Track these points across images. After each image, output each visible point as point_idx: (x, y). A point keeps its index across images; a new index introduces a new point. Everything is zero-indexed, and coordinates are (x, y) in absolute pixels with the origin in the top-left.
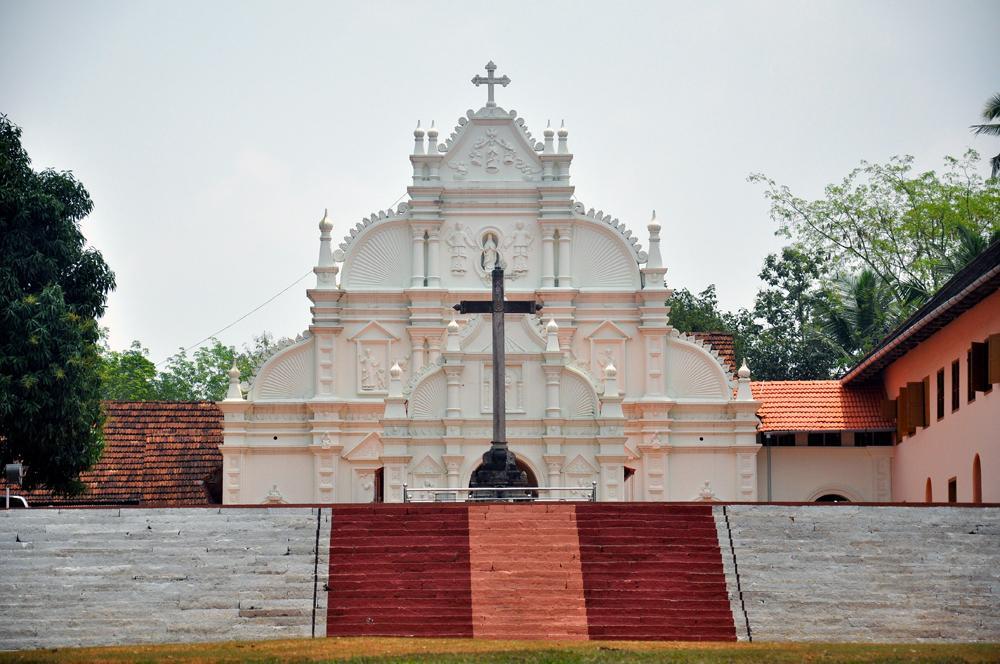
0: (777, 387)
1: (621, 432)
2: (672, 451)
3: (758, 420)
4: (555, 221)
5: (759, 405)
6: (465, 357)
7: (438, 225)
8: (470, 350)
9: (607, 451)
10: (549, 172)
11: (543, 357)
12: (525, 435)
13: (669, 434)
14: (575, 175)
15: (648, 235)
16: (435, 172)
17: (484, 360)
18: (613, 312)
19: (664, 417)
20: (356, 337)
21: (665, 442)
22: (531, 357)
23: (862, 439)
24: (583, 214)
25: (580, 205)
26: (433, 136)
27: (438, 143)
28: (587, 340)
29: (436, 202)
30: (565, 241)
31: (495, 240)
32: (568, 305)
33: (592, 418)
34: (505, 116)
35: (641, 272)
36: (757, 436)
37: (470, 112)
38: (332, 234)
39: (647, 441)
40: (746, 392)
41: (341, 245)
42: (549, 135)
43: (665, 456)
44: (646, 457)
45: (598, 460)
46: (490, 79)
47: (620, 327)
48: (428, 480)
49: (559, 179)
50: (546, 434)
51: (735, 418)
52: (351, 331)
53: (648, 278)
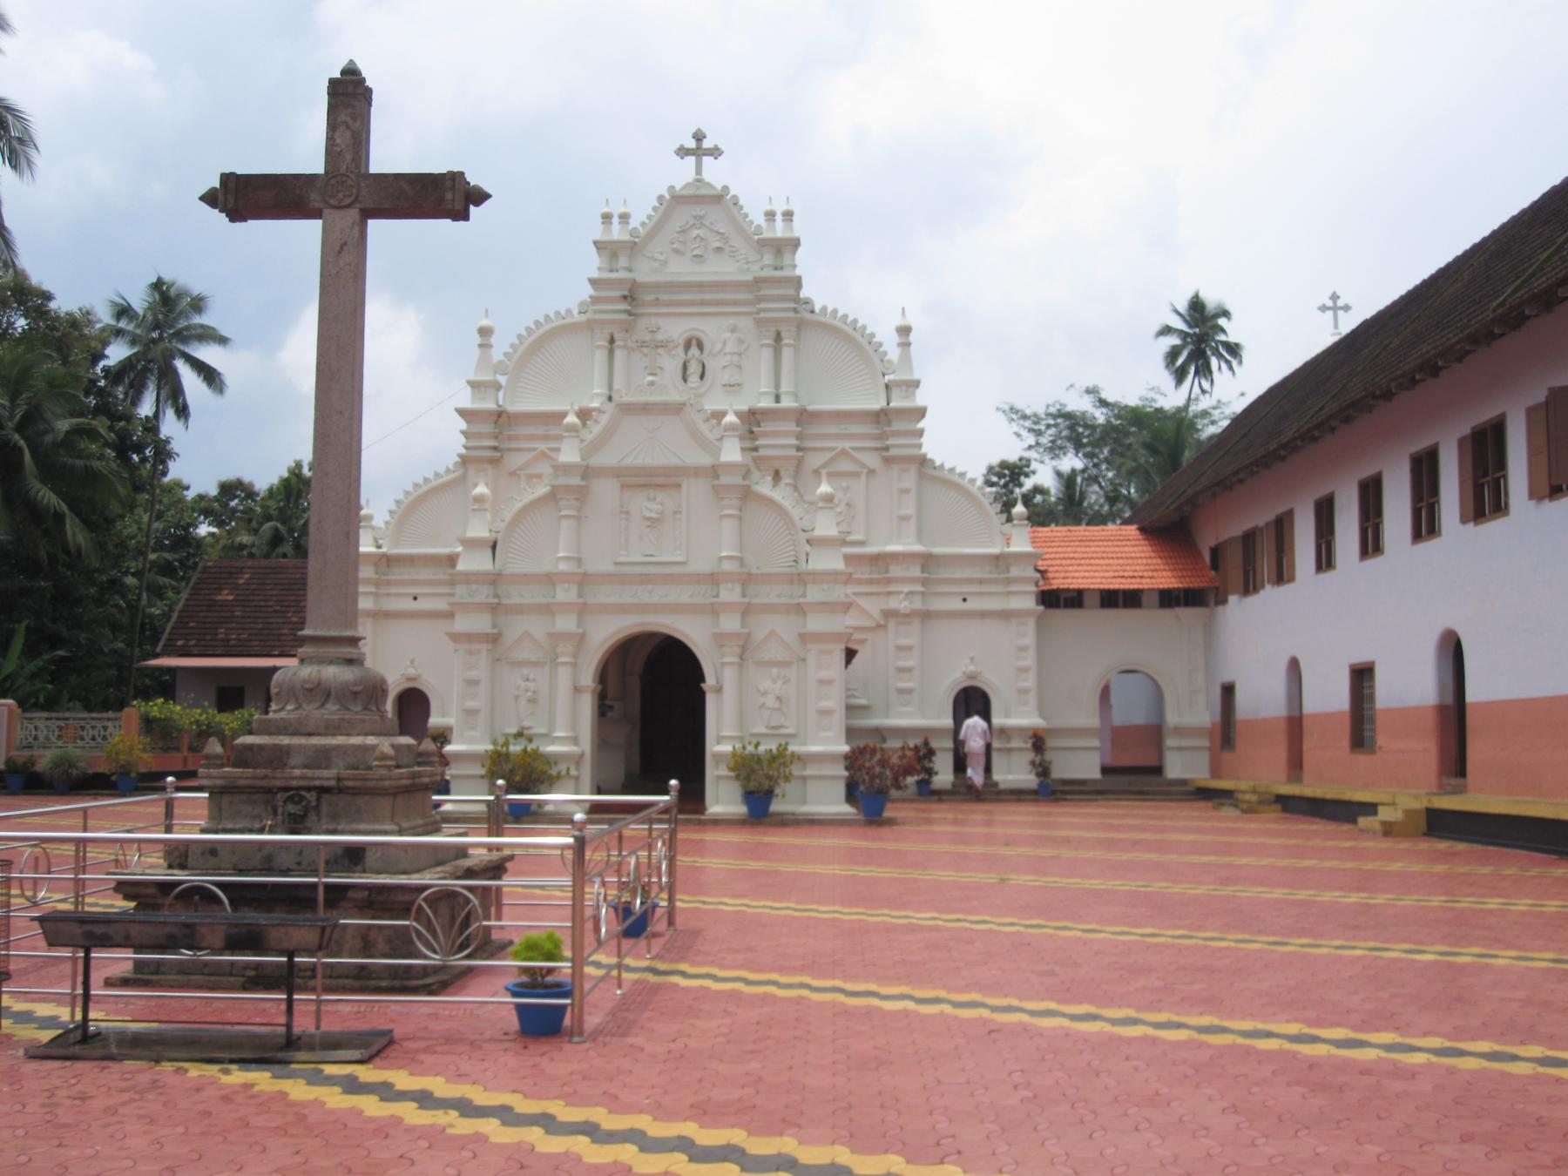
0: (1059, 534)
1: (839, 593)
2: (926, 616)
3: (1038, 575)
4: (775, 320)
5: (1037, 556)
6: (587, 472)
7: (628, 328)
8: (597, 461)
9: (816, 623)
10: (768, 259)
11: (714, 471)
12: (685, 598)
13: (923, 594)
14: (804, 263)
15: (896, 338)
16: (623, 261)
17: (618, 476)
18: (851, 437)
19: (916, 571)
20: (521, 468)
21: (918, 604)
22: (696, 472)
23: (1168, 599)
24: (812, 312)
25: (807, 302)
26: (624, 217)
27: (630, 227)
28: (817, 472)
29: (625, 297)
30: (787, 345)
31: (700, 346)
32: (792, 427)
33: (794, 570)
34: (712, 192)
35: (887, 386)
36: (1037, 596)
37: (671, 188)
38: (494, 340)
39: (894, 603)
40: (1021, 541)
41: (506, 354)
42: (770, 215)
43: (916, 624)
44: (892, 624)
45: (804, 638)
46: (699, 149)
47: (859, 456)
48: (525, 671)
49: (782, 268)
50: (717, 596)
51: (1008, 572)
52: (515, 461)
53: (895, 393)
